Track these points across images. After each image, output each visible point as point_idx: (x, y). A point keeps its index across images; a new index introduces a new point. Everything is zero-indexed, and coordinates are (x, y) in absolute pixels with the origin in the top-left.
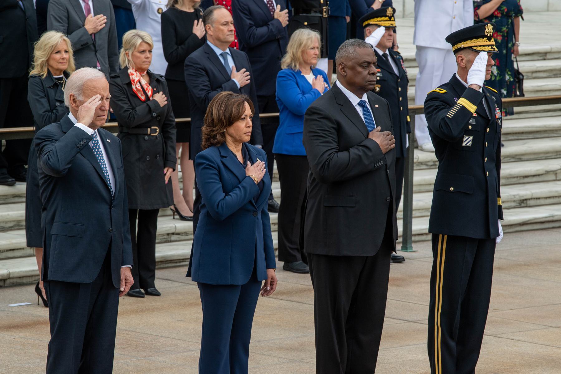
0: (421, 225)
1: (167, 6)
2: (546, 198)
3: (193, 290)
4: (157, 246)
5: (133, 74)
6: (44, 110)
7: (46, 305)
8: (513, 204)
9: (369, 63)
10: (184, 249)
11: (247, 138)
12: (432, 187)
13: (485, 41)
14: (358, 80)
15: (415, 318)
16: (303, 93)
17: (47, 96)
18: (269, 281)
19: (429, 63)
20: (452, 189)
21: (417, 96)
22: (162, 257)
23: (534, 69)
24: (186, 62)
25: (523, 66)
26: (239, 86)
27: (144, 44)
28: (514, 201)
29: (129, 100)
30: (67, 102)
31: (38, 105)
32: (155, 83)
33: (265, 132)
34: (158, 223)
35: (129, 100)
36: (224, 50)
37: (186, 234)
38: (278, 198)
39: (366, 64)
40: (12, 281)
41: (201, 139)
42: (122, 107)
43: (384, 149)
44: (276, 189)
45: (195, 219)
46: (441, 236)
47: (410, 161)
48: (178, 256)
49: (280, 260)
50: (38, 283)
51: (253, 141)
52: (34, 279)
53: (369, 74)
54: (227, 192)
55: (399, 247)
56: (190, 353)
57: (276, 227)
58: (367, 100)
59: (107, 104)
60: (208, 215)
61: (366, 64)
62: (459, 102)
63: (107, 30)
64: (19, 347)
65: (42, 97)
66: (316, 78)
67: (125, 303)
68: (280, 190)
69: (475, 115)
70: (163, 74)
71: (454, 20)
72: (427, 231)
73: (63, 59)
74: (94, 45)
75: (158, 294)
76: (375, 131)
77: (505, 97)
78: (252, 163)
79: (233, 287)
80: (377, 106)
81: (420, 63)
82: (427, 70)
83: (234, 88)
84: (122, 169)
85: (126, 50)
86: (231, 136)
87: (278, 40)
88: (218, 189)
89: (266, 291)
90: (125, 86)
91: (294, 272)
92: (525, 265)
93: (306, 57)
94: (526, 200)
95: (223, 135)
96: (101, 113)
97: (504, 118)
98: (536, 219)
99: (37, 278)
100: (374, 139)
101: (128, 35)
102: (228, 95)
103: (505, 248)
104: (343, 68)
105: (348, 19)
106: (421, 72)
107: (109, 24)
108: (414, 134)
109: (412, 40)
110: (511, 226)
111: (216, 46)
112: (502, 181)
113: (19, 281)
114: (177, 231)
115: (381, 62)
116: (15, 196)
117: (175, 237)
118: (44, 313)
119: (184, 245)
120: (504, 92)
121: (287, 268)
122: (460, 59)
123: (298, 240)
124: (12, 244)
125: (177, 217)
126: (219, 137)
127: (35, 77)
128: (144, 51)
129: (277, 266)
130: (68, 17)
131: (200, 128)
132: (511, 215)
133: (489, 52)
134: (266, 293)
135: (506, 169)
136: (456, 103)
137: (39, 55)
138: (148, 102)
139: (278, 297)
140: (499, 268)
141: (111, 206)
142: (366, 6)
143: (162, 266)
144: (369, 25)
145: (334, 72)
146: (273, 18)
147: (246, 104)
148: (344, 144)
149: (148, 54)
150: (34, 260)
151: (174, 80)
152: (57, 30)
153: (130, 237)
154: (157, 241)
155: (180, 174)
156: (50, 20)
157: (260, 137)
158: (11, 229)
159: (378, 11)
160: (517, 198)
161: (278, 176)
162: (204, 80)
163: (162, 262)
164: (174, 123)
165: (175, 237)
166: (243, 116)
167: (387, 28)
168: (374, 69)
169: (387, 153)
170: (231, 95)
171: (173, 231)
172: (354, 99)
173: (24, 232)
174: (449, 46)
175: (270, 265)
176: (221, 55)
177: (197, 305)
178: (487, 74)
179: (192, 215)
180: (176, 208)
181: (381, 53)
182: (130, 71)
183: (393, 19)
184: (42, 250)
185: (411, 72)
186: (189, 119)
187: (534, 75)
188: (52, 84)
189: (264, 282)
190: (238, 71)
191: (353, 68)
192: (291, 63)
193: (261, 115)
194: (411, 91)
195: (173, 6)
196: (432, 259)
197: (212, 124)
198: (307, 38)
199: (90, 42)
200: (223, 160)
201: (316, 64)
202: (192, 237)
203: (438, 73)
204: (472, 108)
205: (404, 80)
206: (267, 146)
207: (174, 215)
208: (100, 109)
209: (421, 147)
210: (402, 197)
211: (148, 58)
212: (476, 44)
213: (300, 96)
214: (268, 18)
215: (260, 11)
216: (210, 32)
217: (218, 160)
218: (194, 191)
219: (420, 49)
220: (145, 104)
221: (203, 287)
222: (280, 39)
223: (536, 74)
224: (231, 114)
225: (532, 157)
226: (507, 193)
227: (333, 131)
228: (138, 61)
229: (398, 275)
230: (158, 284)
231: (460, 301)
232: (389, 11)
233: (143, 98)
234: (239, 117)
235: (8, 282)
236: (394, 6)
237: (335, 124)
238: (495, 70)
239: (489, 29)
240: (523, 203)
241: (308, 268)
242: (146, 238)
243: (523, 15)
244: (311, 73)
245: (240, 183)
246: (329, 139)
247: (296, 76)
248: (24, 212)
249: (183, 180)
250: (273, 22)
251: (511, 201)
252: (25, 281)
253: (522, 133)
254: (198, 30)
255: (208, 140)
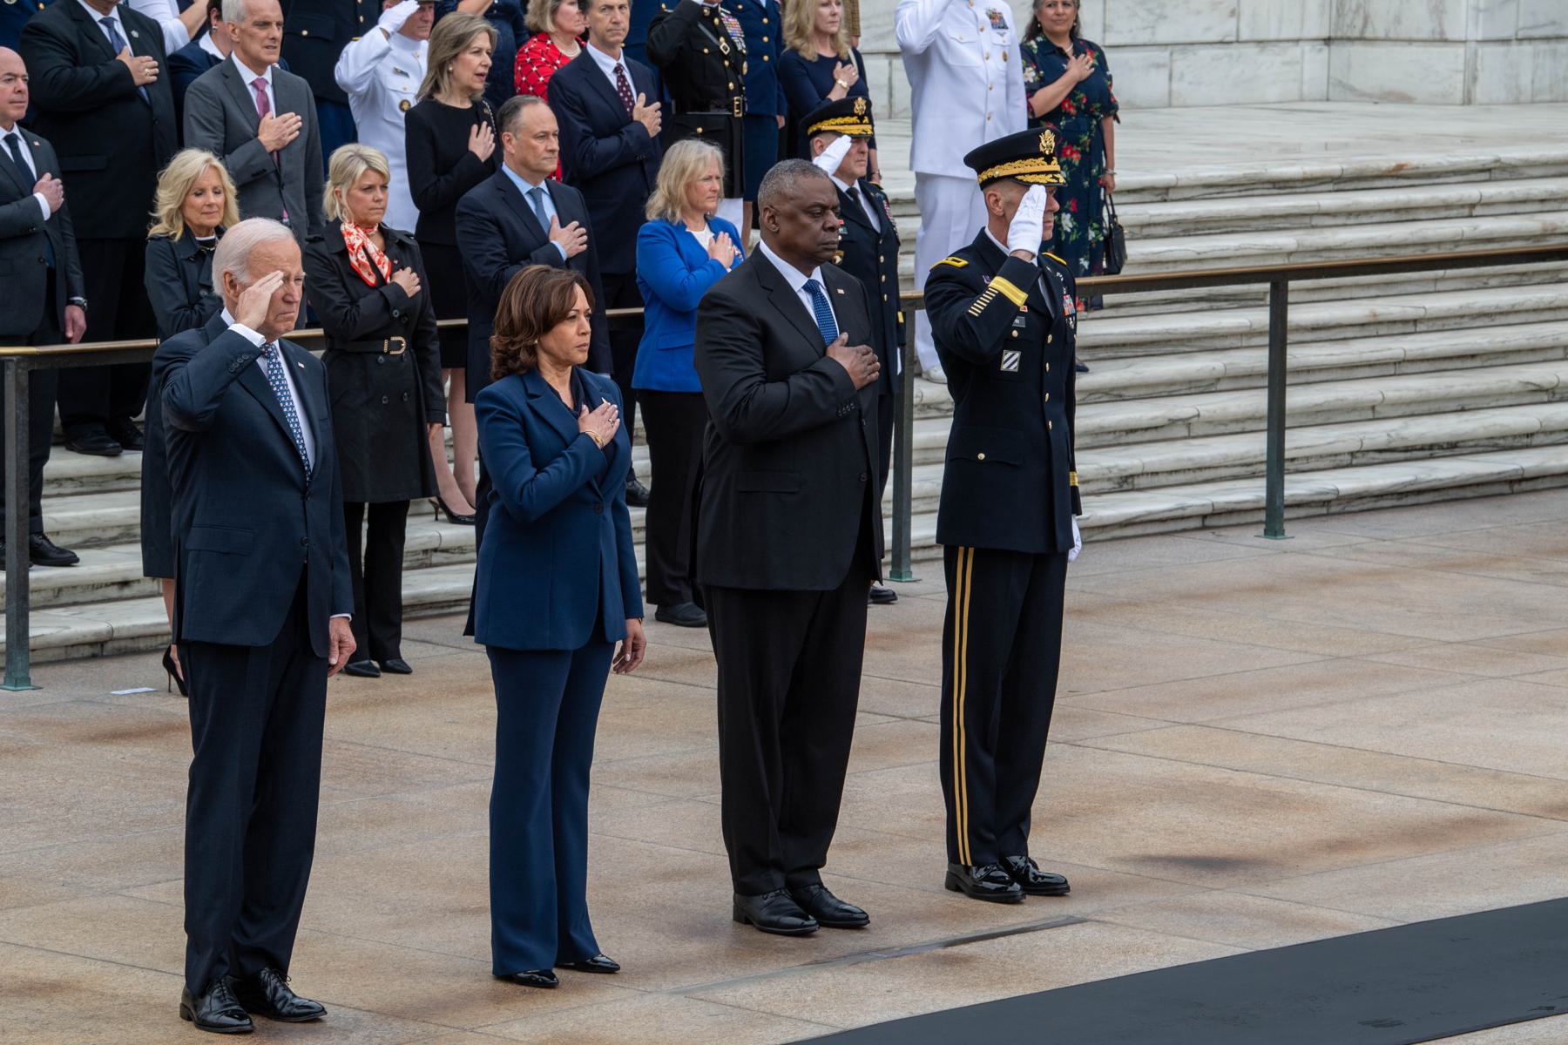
0: (924, 528)
1: (417, 97)
2: (1171, 472)
3: (477, 661)
4: (404, 574)
5: (350, 234)
6: (177, 304)
7: (184, 693)
8: (1107, 485)
9: (824, 208)
10: (459, 580)
11: (582, 357)
12: (943, 455)
13: (1039, 164)
14: (803, 240)
15: (917, 712)
16: (691, 268)
17: (182, 276)
18: (630, 643)
19: (942, 207)
20: (982, 456)
21: (913, 270)
22: (414, 597)
23: (1145, 219)
24: (459, 208)
25: (1127, 213)
26: (565, 257)
27: (371, 173)
28: (1109, 479)
29: (344, 286)
30: (218, 288)
31: (164, 296)
32: (395, 250)
33: (615, 348)
34: (407, 530)
35: (344, 286)
36: (536, 183)
37: (461, 550)
38: (643, 477)
39: (818, 210)
40: (116, 644)
41: (488, 362)
42: (330, 301)
43: (858, 380)
44: (641, 459)
45: (478, 521)
46: (961, 549)
47: (906, 402)
48: (446, 593)
49: (649, 601)
50: (169, 650)
51: (592, 364)
52: (160, 640)
53: (824, 228)
54: (540, 466)
55: (886, 572)
56: (470, 786)
57: (642, 536)
58: (821, 280)
59: (297, 291)
60: (502, 511)
61: (818, 210)
62: (992, 284)
63: (302, 143)
64: (133, 775)
65: (173, 280)
66: (716, 238)
67: (339, 688)
68: (648, 462)
69: (1024, 309)
70: (413, 231)
71: (989, 123)
72: (934, 541)
73: (210, 205)
74: (277, 173)
75: (406, 671)
76: (837, 343)
77: (1088, 273)
78: (592, 408)
79: (555, 654)
80: (841, 291)
81: (923, 208)
82: (937, 223)
83: (554, 258)
84: (329, 422)
85: (336, 185)
86: (548, 352)
87: (641, 163)
88: (522, 460)
89: (623, 663)
90: (337, 259)
91: (678, 624)
92: (1129, 604)
93: (694, 194)
94: (1132, 476)
95: (532, 351)
96: (284, 307)
97: (1082, 314)
98: (1150, 513)
99: (165, 639)
100: (837, 359)
101: (340, 154)
102: (541, 271)
103: (1087, 574)
104: (772, 217)
105: (782, 121)
106: (926, 226)
107: (306, 134)
108: (912, 347)
109: (907, 163)
110: (1103, 527)
111: (520, 175)
112: (1078, 442)
113: (130, 644)
114: (444, 545)
115: (847, 206)
116: (121, 477)
117: (441, 558)
118: (181, 708)
119: (456, 572)
120: (1085, 263)
121: (661, 617)
122: (993, 199)
123: (687, 563)
124: (117, 571)
125: (443, 516)
126: (523, 356)
127: (160, 239)
128: (371, 188)
129: (645, 612)
130: (226, 120)
131: (486, 339)
132: (1103, 507)
133: (1047, 185)
134: (624, 666)
135: (1086, 418)
136: (986, 287)
137: (166, 199)
138: (383, 289)
139: (647, 674)
140: (1081, 612)
141: (304, 492)
142: (815, 93)
143: (414, 614)
144: (819, 132)
145: (756, 226)
146: (631, 119)
147: (578, 289)
148: (776, 366)
149: (379, 194)
150: (160, 603)
151: (432, 244)
152: (203, 147)
153: (346, 558)
154: (404, 565)
155: (448, 431)
156: (191, 126)
157: (606, 357)
158: (113, 541)
159: (840, 102)
160: (1115, 473)
161: (643, 433)
162: (495, 243)
163: (412, 606)
164: (435, 331)
165: (441, 558)
166: (572, 313)
167: (856, 139)
168: (833, 219)
169: (863, 389)
170: (547, 271)
171: (435, 545)
172: (796, 279)
173: (138, 548)
174: (970, 173)
175: (633, 611)
176: (529, 193)
177: (484, 690)
178: (1045, 229)
179: (473, 512)
180: (439, 499)
181: (844, 187)
182: (346, 227)
183: (866, 120)
184: (173, 582)
185: (906, 226)
186: (465, 321)
187: (1146, 231)
188: (193, 253)
189: (619, 644)
190: (563, 225)
191: (792, 217)
192: (666, 209)
193: (609, 312)
194: (905, 264)
195: (430, 96)
196: (946, 597)
197: (511, 330)
198: (697, 160)
199: (270, 169)
200: (532, 402)
201: (714, 210)
202: (474, 556)
203: (962, 227)
204: (1018, 297)
205: (889, 242)
206: (622, 373)
207: (437, 513)
208: (283, 299)
209: (928, 373)
210: (891, 473)
211: (379, 201)
212: (1022, 170)
213: (685, 273)
214: (621, 119)
215: (603, 104)
216: (509, 148)
217: (520, 402)
218: (477, 465)
219: (923, 179)
220: (374, 296)
221: (496, 654)
222: (643, 161)
223: (1148, 230)
224: (547, 309)
225: (1143, 392)
226: (1087, 464)
227: (753, 340)
228: (359, 208)
229: (885, 629)
230: (407, 651)
231: (1001, 678)
232: (860, 104)
233: (372, 280)
234: (563, 315)
235: (109, 646)
236: (872, 95)
237: (755, 326)
238: (1067, 222)
239: (1047, 141)
240: (1126, 483)
241: (704, 617)
242: (388, 556)
243: (1119, 113)
244: (707, 228)
245: (567, 446)
246: (747, 357)
247: (676, 234)
248: (136, 509)
249: (454, 444)
250: (631, 127)
251: (1102, 480)
252: (142, 644)
253: (1124, 345)
254: (481, 143)
255: (503, 362)
